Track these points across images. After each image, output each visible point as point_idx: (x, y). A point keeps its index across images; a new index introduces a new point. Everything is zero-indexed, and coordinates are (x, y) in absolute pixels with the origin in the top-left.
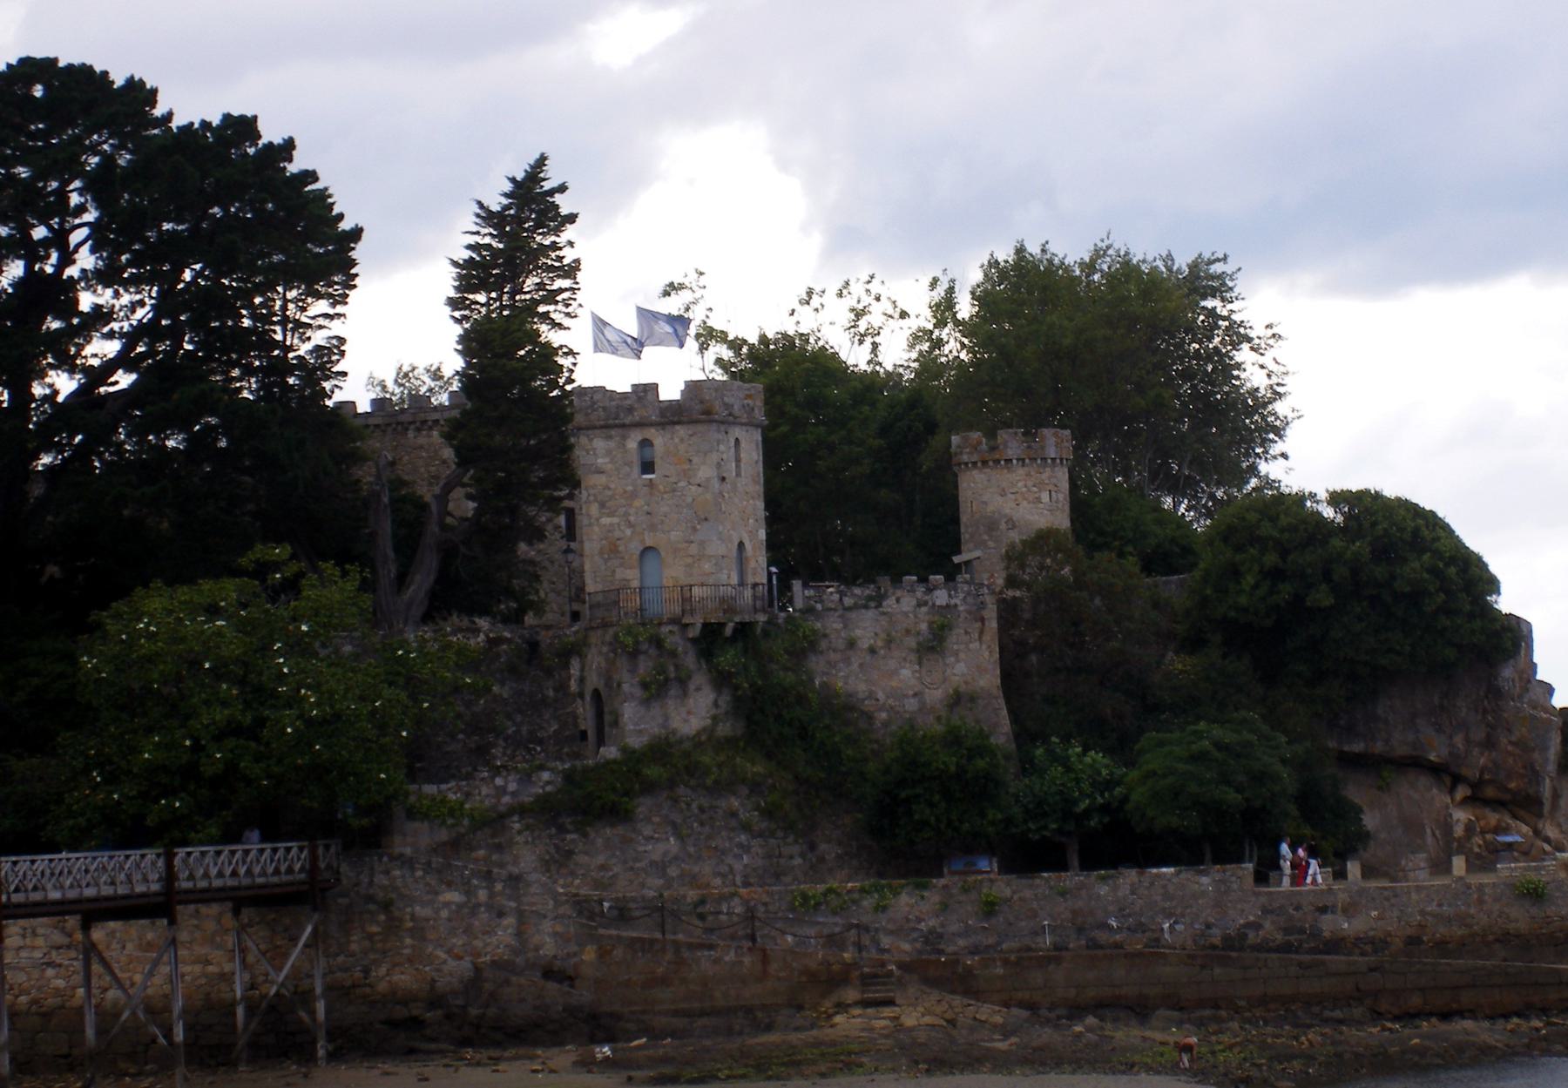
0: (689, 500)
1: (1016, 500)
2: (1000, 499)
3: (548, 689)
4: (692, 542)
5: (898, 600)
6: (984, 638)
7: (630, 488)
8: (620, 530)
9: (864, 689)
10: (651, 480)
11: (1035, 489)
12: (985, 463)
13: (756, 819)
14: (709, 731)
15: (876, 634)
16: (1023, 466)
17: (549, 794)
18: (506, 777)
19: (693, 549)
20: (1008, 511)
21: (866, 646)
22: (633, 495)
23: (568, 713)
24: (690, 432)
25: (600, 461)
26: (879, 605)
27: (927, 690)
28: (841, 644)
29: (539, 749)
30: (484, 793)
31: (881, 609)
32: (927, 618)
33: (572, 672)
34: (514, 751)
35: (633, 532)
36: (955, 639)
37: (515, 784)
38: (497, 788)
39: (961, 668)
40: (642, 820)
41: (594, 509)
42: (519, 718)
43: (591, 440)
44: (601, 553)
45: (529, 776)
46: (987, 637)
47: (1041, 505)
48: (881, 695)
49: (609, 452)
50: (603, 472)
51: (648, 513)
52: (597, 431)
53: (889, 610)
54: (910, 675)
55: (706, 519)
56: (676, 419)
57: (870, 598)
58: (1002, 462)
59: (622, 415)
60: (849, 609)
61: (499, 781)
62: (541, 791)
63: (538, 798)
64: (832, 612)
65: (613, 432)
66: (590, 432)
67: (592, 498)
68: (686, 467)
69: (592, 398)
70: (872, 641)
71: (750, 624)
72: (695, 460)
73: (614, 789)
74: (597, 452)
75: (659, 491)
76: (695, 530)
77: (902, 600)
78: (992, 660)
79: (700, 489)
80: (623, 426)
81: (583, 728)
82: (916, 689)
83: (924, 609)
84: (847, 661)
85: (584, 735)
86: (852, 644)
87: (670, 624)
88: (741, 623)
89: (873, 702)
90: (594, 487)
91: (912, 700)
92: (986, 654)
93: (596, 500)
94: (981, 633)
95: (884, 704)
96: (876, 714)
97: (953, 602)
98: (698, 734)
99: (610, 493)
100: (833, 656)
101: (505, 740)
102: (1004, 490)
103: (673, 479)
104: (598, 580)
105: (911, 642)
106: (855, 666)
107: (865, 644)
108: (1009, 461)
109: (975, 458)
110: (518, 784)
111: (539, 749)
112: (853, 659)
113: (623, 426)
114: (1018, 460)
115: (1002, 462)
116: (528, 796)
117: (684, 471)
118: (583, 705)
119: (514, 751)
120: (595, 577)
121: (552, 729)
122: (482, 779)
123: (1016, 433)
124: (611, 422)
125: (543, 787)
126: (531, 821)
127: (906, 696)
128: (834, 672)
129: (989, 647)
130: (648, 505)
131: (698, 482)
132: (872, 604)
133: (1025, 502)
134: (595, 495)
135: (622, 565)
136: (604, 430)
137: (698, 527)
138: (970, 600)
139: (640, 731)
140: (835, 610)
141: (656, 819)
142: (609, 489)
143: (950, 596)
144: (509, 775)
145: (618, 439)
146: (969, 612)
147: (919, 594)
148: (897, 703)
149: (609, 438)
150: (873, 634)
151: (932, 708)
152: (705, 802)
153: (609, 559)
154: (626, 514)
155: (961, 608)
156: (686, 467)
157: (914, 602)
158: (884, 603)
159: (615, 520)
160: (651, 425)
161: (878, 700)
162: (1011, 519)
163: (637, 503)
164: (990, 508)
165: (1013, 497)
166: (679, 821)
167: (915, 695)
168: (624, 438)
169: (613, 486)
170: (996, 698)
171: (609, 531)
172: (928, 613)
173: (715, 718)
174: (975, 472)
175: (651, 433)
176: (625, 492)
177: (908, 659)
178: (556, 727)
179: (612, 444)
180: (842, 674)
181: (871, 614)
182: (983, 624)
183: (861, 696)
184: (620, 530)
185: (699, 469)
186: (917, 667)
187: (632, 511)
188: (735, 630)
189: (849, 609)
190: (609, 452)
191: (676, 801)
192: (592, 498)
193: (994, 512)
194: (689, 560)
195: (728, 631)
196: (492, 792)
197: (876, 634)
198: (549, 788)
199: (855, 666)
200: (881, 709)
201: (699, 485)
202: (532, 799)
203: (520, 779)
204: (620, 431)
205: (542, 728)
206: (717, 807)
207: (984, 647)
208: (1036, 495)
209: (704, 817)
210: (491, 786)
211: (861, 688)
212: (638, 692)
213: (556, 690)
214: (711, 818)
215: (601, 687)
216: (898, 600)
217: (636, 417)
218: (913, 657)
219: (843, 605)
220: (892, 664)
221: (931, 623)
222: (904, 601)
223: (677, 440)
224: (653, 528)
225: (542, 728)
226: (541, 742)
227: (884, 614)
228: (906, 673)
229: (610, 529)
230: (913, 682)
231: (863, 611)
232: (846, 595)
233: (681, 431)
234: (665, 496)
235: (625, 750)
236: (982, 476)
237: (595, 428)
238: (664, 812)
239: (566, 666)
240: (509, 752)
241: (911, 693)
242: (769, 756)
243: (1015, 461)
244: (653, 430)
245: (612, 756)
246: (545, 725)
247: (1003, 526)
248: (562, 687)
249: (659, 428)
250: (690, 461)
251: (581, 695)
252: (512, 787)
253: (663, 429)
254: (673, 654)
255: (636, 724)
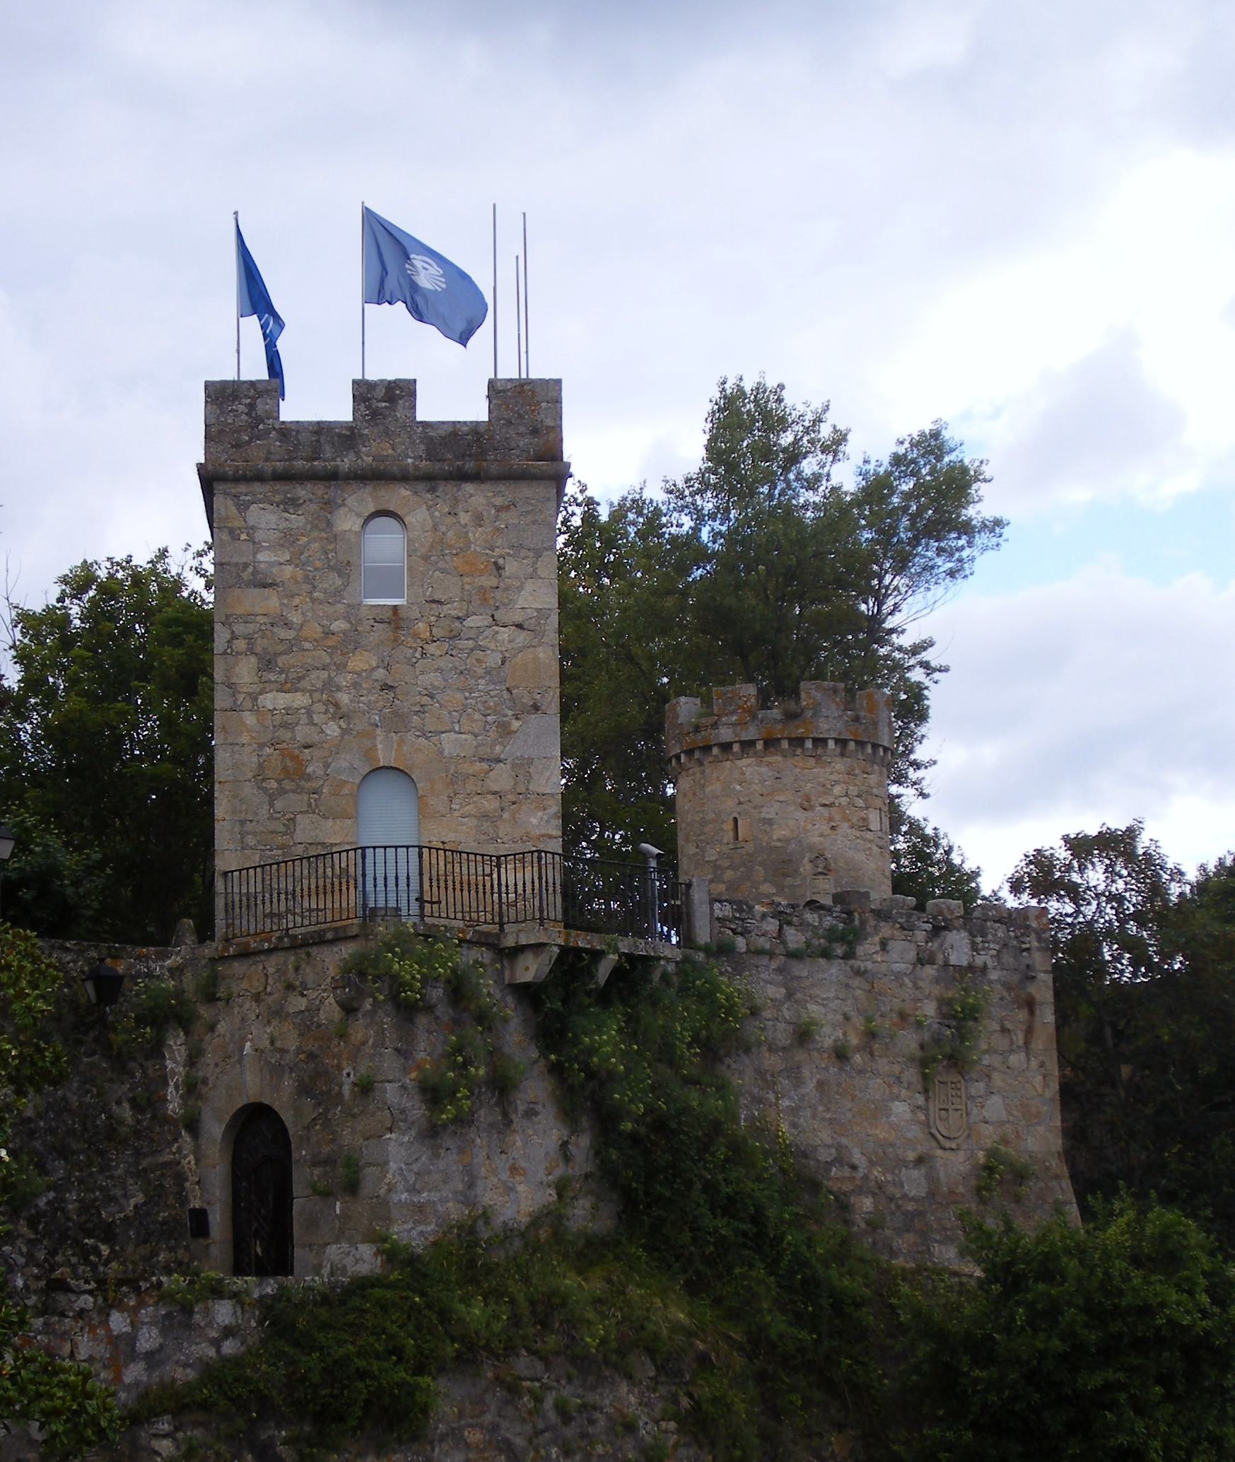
0: (493, 660)
1: (831, 819)
2: (801, 815)
3: (119, 1103)
4: (499, 761)
5: (884, 944)
6: (1033, 1046)
7: (339, 625)
8: (311, 723)
9: (829, 1141)
10: (395, 608)
11: (860, 802)
12: (771, 743)
13: (673, 1439)
14: (551, 1218)
15: (847, 1018)
16: (843, 755)
17: (236, 1361)
18: (134, 1311)
19: (501, 778)
20: (816, 839)
21: (828, 1043)
22: (351, 642)
23: (165, 1165)
24: (499, 501)
25: (262, 557)
26: (849, 955)
27: (939, 1152)
28: (782, 1034)
29: (105, 1250)
30: (83, 1353)
31: (852, 962)
32: (936, 990)
33: (170, 1065)
34: (53, 1253)
35: (345, 732)
36: (987, 1036)
37: (155, 1332)
38: (113, 1340)
39: (995, 1107)
40: (443, 1438)
41: (245, 672)
42: (59, 1169)
43: (243, 507)
44: (260, 776)
45: (187, 1310)
46: (1039, 1044)
47: (869, 835)
48: (857, 1157)
49: (288, 538)
50: (271, 585)
51: (386, 687)
52: (258, 487)
53: (869, 965)
54: (908, 1116)
55: (536, 708)
56: (470, 466)
57: (832, 936)
58: (809, 744)
59: (328, 451)
60: (795, 955)
61: (118, 1322)
62: (212, 1353)
63: (211, 1373)
64: (764, 960)
65: (301, 492)
66: (242, 488)
67: (240, 645)
68: (489, 581)
69: (252, 407)
70: (840, 1033)
71: (646, 959)
72: (511, 567)
73: (397, 1352)
74: (259, 535)
75: (416, 636)
76: (505, 731)
77: (891, 944)
78: (1048, 1094)
79: (522, 637)
80: (332, 477)
81: (196, 1204)
82: (920, 1149)
83: (930, 971)
84: (794, 1073)
85: (199, 1222)
86: (804, 1035)
87: (480, 944)
88: (630, 958)
89: (847, 1172)
90: (248, 618)
91: (915, 1173)
92: (1038, 1079)
93: (251, 651)
94: (1029, 1032)
95: (866, 1177)
96: (852, 1200)
97: (979, 961)
98: (535, 1222)
99: (290, 634)
100: (771, 1061)
101: (33, 1223)
102: (809, 800)
103: (453, 610)
104: (251, 840)
105: (909, 1041)
106: (810, 1087)
107: (828, 1037)
108: (820, 742)
109: (751, 733)
110: (164, 1332)
111: (105, 1250)
112: (806, 1072)
113: (332, 477)
114: (837, 741)
115: (809, 744)
116: (186, 1365)
117: (482, 590)
118: (197, 1151)
119: (53, 1253)
120: (243, 835)
121: (133, 1202)
122: (81, 1314)
123: (835, 691)
124: (300, 464)
125: (216, 1343)
126: (198, 1433)
127: (904, 1163)
128: (771, 1096)
129: (1042, 1065)
130: (387, 668)
131: (518, 618)
132: (839, 950)
133: (846, 825)
134: (249, 638)
135: (310, 810)
136: (279, 486)
137: (516, 724)
138: (1008, 958)
139: (420, 1208)
140: (771, 955)
141: (474, 1436)
142: (287, 625)
143: (974, 948)
144: (141, 1304)
145: (313, 507)
146: (1008, 987)
147: (920, 936)
148: (889, 1178)
149: (291, 504)
150: (840, 1017)
151: (951, 1192)
152: (571, 1394)
153: (282, 792)
154: (330, 686)
155: (994, 976)
156: (489, 581)
157: (912, 955)
158: (860, 950)
159: (300, 700)
160: (404, 478)
161: (854, 1167)
162: (820, 855)
163: (359, 662)
164: (779, 833)
165: (825, 812)
166: (519, 1442)
167: (920, 1161)
168: (329, 505)
169: (296, 618)
170: (1057, 1177)
171: (284, 725)
172: (937, 981)
173: (561, 1188)
174: (910, 600)
175: (398, 496)
176: (329, 633)
177: (905, 1078)
178: (140, 1198)
179: (297, 521)
180: (785, 1103)
181: (834, 970)
182: (1032, 1012)
183: (825, 1155)
184: (311, 723)
185: (521, 588)
186: (920, 1100)
187: (344, 680)
188: (617, 972)
189: (795, 955)
190: (288, 538)
191: (513, 1389)
192: (240, 645)
193: (787, 841)
194: (490, 804)
195: (603, 971)
196: (102, 1351)
197: (847, 1018)
198: (229, 1347)
199: (810, 1087)
200: (860, 1190)
201: (520, 626)
202: (191, 1374)
203: (168, 1316)
204: (320, 489)
205: (110, 1199)
206: (595, 1408)
207: (1034, 1063)
208: (863, 814)
209: (570, 1432)
210: (101, 1332)
211: (820, 1137)
212: (417, 1110)
213: (136, 1106)
214: (584, 1435)
215: (283, 1100)
216: (884, 944)
217: (367, 458)
218: (912, 1075)
219: (784, 943)
220: (876, 1087)
221: (941, 1001)
222: (896, 946)
223: (464, 518)
224: (397, 722)
225: (110, 1199)
226: (108, 1234)
227: (858, 973)
228: (900, 1109)
229: (287, 721)
230: (915, 1132)
231: (822, 961)
232: (790, 923)
233: (477, 496)
234: (431, 648)
235: (392, 1254)
236: (764, 769)
237: (259, 478)
238: (488, 1418)
239: (156, 1050)
240: (41, 1255)
241: (911, 1156)
242: (693, 1289)
243: (831, 744)
244: (404, 492)
245: (364, 1269)
246: (118, 1192)
247: (806, 868)
248: (149, 1102)
249: (421, 486)
250: (499, 568)
251: (193, 1125)
252: (148, 1339)
253: (433, 490)
254: (483, 1018)
255: (413, 1190)
